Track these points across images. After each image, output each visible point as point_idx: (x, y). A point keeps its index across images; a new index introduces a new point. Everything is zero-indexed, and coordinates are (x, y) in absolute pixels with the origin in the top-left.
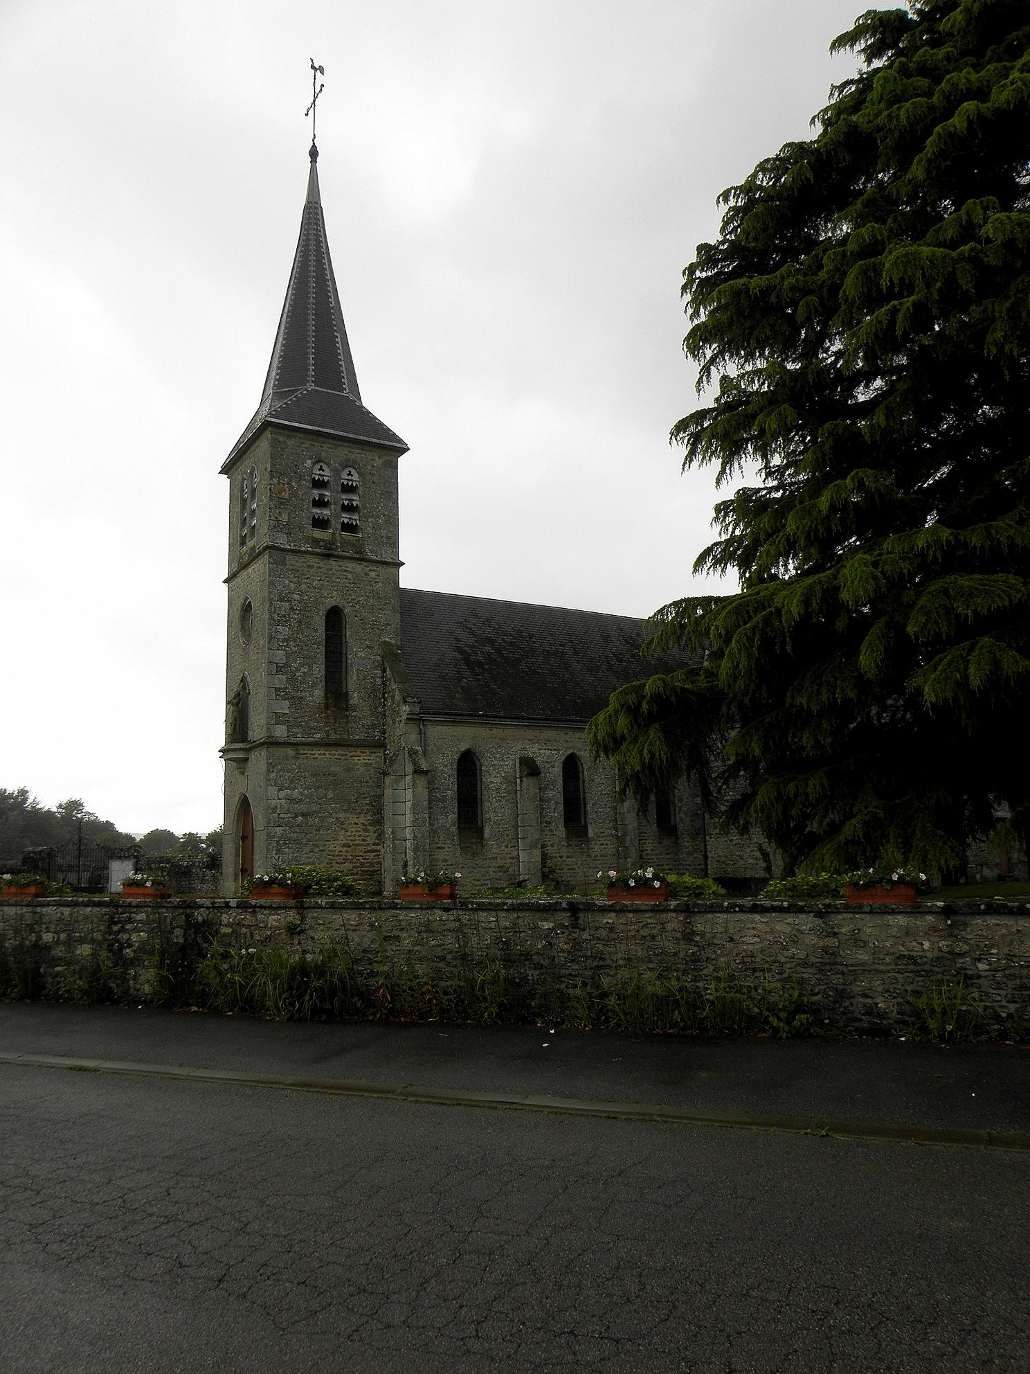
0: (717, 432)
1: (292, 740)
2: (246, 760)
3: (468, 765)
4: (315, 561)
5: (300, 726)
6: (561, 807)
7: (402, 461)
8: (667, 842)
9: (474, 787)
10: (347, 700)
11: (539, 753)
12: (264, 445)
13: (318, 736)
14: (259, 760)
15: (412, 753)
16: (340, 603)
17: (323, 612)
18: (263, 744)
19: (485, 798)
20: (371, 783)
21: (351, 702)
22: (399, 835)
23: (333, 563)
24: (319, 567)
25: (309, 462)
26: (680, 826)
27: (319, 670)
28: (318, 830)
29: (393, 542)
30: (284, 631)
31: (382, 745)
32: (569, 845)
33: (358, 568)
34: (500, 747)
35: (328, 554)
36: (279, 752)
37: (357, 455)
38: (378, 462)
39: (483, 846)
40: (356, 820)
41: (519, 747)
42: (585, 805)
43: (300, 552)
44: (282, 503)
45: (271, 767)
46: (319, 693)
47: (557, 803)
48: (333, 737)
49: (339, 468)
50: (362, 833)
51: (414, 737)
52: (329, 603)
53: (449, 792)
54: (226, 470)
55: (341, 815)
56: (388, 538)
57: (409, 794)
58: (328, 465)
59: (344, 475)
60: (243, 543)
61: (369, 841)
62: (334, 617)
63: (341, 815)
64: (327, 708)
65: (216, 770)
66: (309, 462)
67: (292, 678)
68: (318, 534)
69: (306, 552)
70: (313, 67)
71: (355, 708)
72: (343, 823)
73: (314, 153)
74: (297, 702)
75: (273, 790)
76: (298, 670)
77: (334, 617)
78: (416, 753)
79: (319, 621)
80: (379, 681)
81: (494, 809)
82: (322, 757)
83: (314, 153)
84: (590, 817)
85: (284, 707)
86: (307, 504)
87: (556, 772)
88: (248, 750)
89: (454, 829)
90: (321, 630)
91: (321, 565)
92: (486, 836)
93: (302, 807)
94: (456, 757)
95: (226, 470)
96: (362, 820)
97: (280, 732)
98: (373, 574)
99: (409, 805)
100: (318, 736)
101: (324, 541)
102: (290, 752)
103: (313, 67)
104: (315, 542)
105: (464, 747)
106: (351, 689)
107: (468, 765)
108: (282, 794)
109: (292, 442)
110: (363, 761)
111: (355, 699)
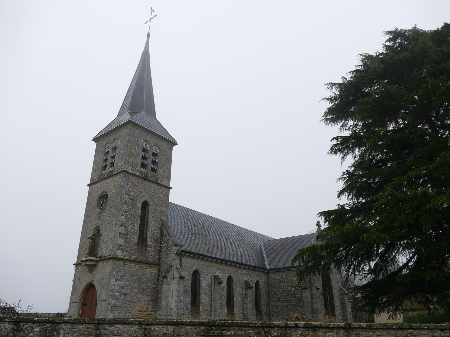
0: (342, 146)
1: (124, 258)
2: (95, 266)
3: (196, 275)
4: (140, 181)
5: (127, 251)
6: (226, 299)
7: (174, 148)
8: (258, 317)
9: (196, 287)
10: (146, 243)
11: (218, 273)
12: (126, 130)
13: (134, 257)
14: (105, 268)
15: (177, 269)
16: (148, 200)
17: (141, 202)
18: (110, 258)
19: (201, 292)
20: (152, 282)
21: (148, 243)
22: (170, 307)
23: (147, 183)
24: (141, 183)
25: (142, 140)
26: (263, 311)
27: (137, 227)
28: (129, 302)
29: (168, 178)
30: (126, 208)
31: (158, 265)
32: (228, 316)
33: (155, 186)
34: (207, 270)
35: (145, 179)
36: (117, 263)
37: (160, 142)
38: (166, 147)
39: (199, 315)
40: (145, 299)
41: (213, 271)
42: (233, 299)
43: (136, 175)
44: (131, 154)
45: (113, 269)
46: (136, 237)
47: (224, 297)
48: (140, 258)
49: (153, 145)
50: (147, 305)
51: (178, 261)
52: (144, 199)
53: (189, 288)
54: (95, 140)
55: (139, 296)
56: (167, 177)
57: (176, 287)
58: (149, 143)
59: (154, 148)
60: (105, 168)
61: (149, 309)
62: (145, 205)
63: (139, 296)
64: (138, 245)
65: (70, 272)
66: (142, 140)
67: (126, 229)
68: (143, 170)
69: (138, 176)
70: (151, 9)
71: (149, 245)
72: (139, 300)
73: (148, 36)
74: (127, 240)
75: (113, 281)
76: (129, 226)
77: (145, 205)
78: (179, 269)
79: (139, 206)
80: (159, 236)
81: (204, 298)
82: (134, 267)
83: (148, 36)
84: (235, 304)
85: (121, 241)
86: (140, 157)
87: (225, 283)
88: (97, 261)
89: (189, 305)
90: (140, 209)
91: (142, 182)
92: (200, 310)
93: (124, 291)
94: (192, 272)
95: (95, 140)
96: (147, 299)
97: (119, 253)
98: (160, 190)
99: (175, 292)
100: (134, 257)
101: (144, 173)
102: (122, 263)
103: (151, 9)
104: (141, 173)
105: (195, 268)
106: (148, 237)
107: (196, 275)
108: (117, 283)
109: (137, 131)
110: (150, 272)
111: (149, 242)
